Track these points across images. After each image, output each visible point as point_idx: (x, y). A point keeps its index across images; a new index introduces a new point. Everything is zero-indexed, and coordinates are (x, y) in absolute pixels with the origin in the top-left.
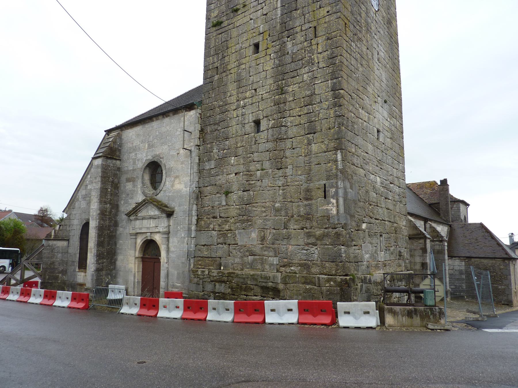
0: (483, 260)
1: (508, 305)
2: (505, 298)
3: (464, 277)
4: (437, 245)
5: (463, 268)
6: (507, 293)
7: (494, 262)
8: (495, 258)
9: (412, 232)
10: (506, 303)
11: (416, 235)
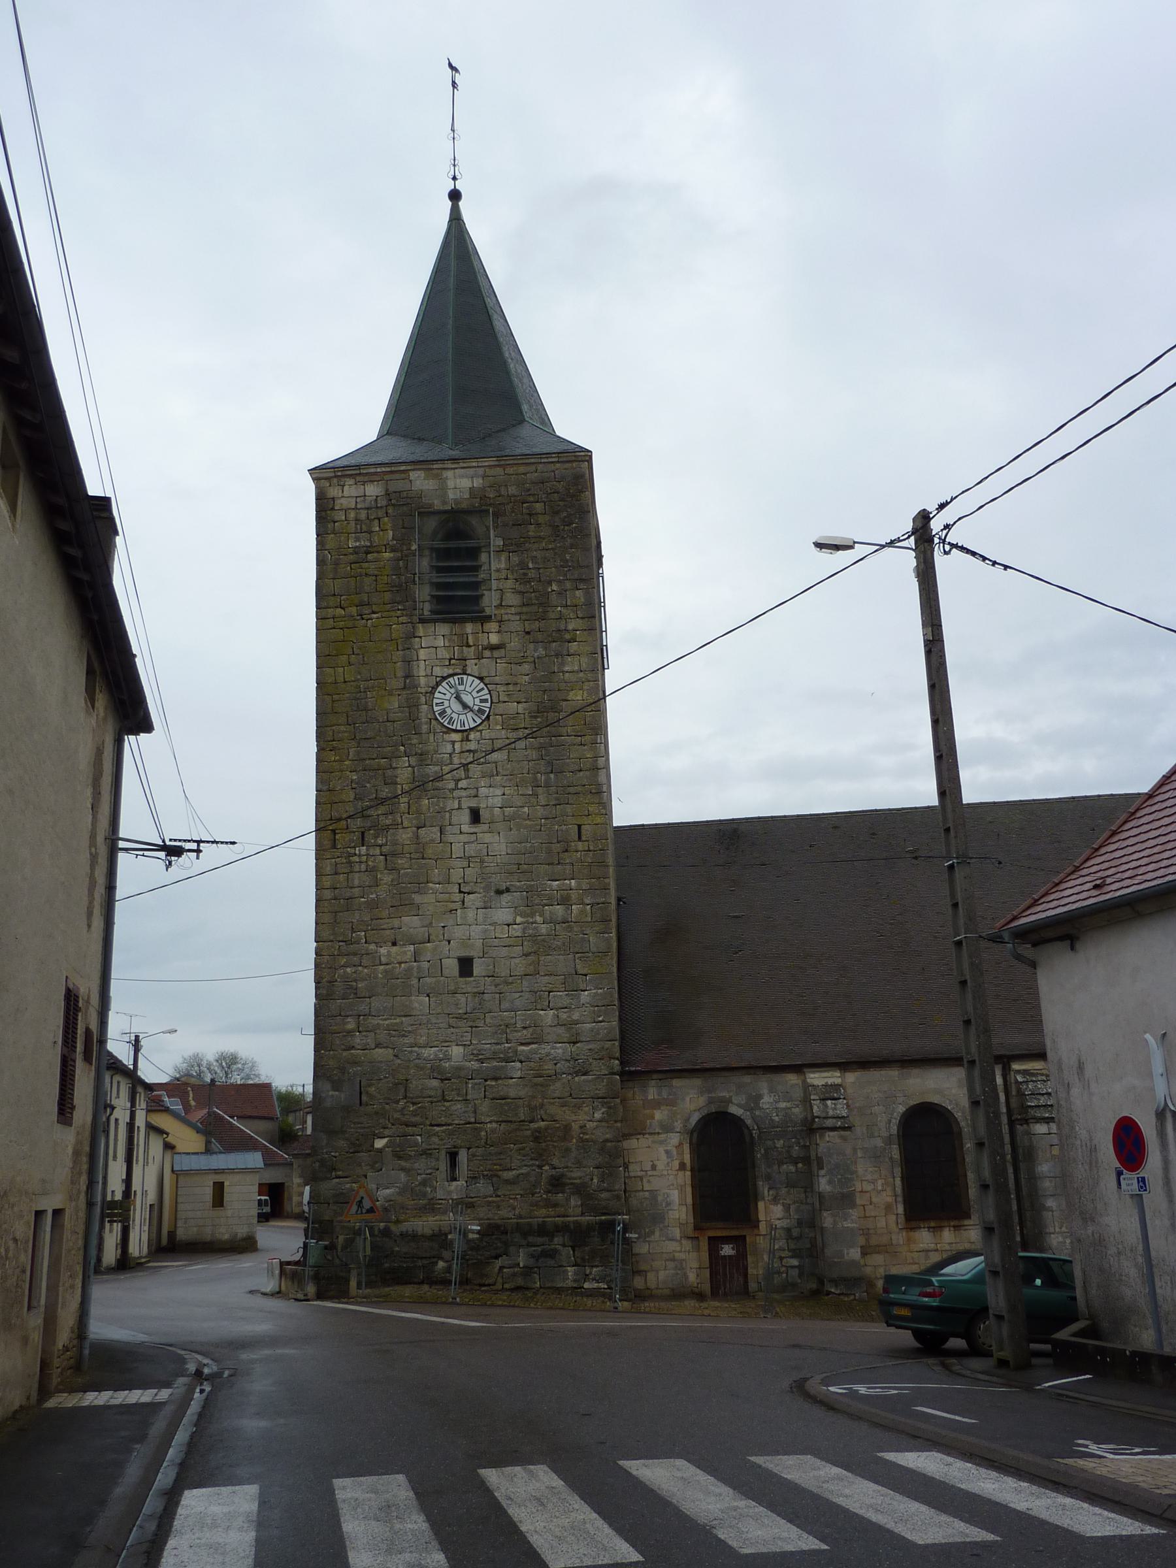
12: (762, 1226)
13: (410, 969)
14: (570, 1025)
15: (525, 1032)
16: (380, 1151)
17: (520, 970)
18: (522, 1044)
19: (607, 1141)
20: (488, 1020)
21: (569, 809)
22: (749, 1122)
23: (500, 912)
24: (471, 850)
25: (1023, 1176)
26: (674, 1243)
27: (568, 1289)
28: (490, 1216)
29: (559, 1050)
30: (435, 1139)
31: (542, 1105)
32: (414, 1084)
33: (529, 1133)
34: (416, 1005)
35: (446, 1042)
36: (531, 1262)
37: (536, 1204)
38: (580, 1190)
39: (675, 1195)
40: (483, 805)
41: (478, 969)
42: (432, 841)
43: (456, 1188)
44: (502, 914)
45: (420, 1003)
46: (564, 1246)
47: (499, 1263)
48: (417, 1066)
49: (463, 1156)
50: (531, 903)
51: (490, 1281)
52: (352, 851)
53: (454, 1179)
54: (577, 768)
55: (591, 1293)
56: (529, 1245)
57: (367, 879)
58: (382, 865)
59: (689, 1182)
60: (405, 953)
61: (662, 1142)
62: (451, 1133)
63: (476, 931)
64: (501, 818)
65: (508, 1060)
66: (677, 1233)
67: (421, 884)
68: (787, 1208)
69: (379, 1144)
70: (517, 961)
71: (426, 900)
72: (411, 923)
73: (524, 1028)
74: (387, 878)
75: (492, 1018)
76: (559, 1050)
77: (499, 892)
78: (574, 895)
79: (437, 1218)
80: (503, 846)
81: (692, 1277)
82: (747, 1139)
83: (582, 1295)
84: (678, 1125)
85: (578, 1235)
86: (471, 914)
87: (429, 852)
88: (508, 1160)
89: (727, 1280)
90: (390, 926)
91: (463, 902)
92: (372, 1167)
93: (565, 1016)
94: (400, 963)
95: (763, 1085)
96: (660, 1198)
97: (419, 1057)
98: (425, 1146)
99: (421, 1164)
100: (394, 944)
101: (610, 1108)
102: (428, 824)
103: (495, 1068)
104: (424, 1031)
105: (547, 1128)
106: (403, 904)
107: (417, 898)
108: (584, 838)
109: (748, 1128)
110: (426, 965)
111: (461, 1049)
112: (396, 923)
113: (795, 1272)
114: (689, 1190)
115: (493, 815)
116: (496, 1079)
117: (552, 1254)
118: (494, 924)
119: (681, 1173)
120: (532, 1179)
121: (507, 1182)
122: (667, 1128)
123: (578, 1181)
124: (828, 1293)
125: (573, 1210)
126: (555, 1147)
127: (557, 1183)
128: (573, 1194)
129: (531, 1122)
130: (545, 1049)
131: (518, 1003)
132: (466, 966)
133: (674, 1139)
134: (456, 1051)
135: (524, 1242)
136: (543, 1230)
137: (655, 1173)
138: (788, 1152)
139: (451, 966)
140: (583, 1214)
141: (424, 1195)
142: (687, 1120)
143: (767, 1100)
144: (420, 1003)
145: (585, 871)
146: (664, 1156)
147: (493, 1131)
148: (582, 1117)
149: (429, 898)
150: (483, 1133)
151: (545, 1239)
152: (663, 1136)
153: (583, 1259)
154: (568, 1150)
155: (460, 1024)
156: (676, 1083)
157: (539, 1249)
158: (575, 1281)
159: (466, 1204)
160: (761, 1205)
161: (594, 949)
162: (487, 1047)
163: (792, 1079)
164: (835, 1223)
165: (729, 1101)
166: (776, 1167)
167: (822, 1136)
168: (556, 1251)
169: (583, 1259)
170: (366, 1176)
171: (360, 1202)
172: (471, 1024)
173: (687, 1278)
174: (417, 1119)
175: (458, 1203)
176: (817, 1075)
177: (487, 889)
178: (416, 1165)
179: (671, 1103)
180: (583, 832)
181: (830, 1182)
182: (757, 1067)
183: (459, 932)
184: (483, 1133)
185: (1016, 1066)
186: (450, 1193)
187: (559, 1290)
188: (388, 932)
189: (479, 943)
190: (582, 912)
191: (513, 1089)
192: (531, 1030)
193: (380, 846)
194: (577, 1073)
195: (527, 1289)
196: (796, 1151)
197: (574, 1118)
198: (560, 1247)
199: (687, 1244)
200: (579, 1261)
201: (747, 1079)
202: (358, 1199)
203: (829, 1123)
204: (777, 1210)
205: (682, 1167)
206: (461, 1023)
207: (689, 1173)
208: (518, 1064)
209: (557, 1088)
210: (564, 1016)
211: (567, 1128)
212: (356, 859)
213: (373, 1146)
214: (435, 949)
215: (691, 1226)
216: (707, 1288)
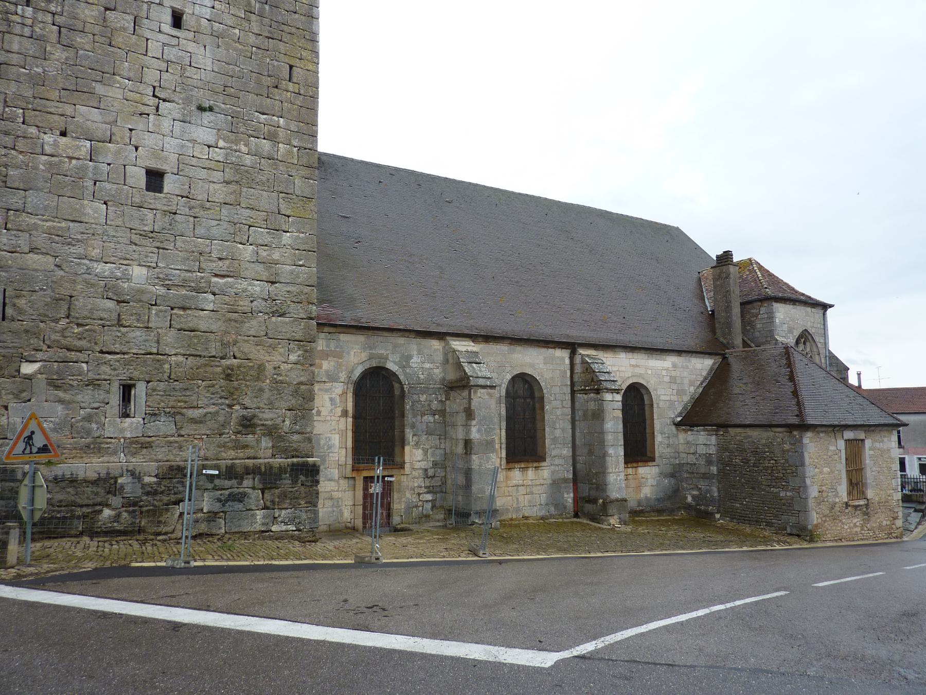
0: (749, 432)
1: (799, 536)
2: (793, 520)
3: (714, 469)
4: (591, 399)
5: (713, 450)
6: (797, 507)
7: (771, 434)
8: (771, 426)
9: (452, 376)
10: (795, 532)
11: (457, 381)
12: (407, 466)
13: (84, 168)
14: (269, 264)
15: (221, 263)
16: (29, 378)
17: (220, 197)
18: (216, 275)
19: (301, 383)
20: (179, 244)
21: (282, 46)
22: (402, 377)
23: (200, 129)
24: (171, 53)
25: (344, 440)
26: (332, 483)
27: (255, 533)
28: (172, 457)
29: (257, 288)
30: (105, 368)
31: (235, 342)
32: (79, 303)
33: (219, 370)
34: (90, 212)
35: (126, 261)
36: (217, 507)
37: (224, 445)
38: (271, 431)
39: (336, 439)
40: (188, 10)
41: (169, 184)
42: (124, 29)
43: (131, 426)
44: (204, 134)
45: (94, 210)
46: (254, 488)
47: (178, 510)
48: (87, 282)
49: (140, 391)
50: (236, 128)
51: (169, 529)
52: (12, 8)
53: (126, 415)
54: (292, 9)
55: (280, 537)
56: (215, 489)
57: (31, 47)
58: (54, 37)
59: (350, 427)
60: (78, 148)
61: (327, 391)
62: (127, 363)
63: (171, 144)
64: (209, 31)
65: (198, 291)
66: (335, 473)
67: (107, 75)
68: (425, 452)
69: (28, 369)
70: (217, 186)
71: (113, 93)
72: (88, 116)
73: (220, 259)
74: (59, 54)
75: (184, 242)
76: (257, 288)
77: (201, 109)
78: (282, 133)
79: (105, 459)
80: (209, 62)
81: (347, 515)
82: (397, 392)
83: (270, 538)
84: (343, 376)
85: (268, 478)
86: (166, 124)
87: (118, 40)
88: (194, 397)
89: (377, 513)
90: (60, 111)
91: (157, 109)
92: (17, 396)
93: (265, 254)
94: (71, 158)
95: (413, 346)
96: (322, 442)
97: (89, 271)
98: (91, 375)
99: (86, 397)
100: (63, 134)
101: (306, 351)
102: (118, 7)
103: (185, 297)
104: (97, 243)
105: (239, 367)
106: (78, 90)
107: (99, 89)
108: (295, 80)
109: (400, 382)
110: (105, 168)
111: (144, 271)
112: (69, 110)
113: (429, 506)
114: (350, 434)
115: (200, 25)
116: (184, 308)
117: (239, 498)
118: (194, 141)
119: (343, 420)
120: (221, 419)
121: (193, 421)
122: (333, 378)
123: (269, 423)
124: (473, 523)
125: (263, 451)
126: (247, 386)
127: (248, 424)
128: (264, 435)
129: (222, 358)
130: (242, 285)
131: (214, 231)
132: (155, 179)
133: (338, 388)
134: (138, 273)
135: (210, 486)
136: (230, 473)
137: (319, 418)
138: (429, 405)
139: (138, 177)
140: (273, 456)
141: (88, 432)
142: (352, 372)
143: (415, 361)
144: (94, 210)
145: (295, 113)
146: (328, 404)
147: (178, 365)
148: (277, 357)
149: (114, 93)
150: (167, 366)
151: (234, 482)
152: (328, 385)
153: (273, 502)
154: (261, 390)
155: (144, 242)
156: (343, 337)
157: (227, 492)
158: (263, 524)
159: (141, 444)
160: (407, 448)
161: (298, 192)
162: (177, 275)
163: (436, 344)
164: (480, 466)
165: (387, 358)
166: (419, 417)
167: (475, 392)
168: (245, 495)
169: (273, 502)
170: (6, 408)
171: (30, 438)
172: (158, 244)
173: (342, 515)
174: (83, 343)
175: (133, 441)
176: (457, 343)
177: (188, 101)
178: (79, 398)
179: (339, 355)
180: (294, 74)
181: (479, 431)
182: (410, 331)
183: (149, 140)
184: (167, 366)
185: (582, 351)
186: (122, 430)
187: (245, 535)
188: (56, 118)
189: (173, 158)
190: (289, 152)
191: (203, 321)
192: (227, 262)
193: (54, 14)
194: (273, 313)
195: (212, 535)
196: (435, 405)
197: (268, 358)
198: (250, 491)
199: (344, 483)
200: (268, 504)
201: (401, 340)
202: (27, 433)
203: (481, 382)
204: (419, 454)
205: (345, 413)
206: (147, 242)
207: (350, 420)
208: (211, 297)
209: (253, 326)
210: (263, 253)
211: (261, 368)
212: (14, 18)
213: (19, 371)
214: (118, 153)
215: (349, 467)
216: (359, 523)
